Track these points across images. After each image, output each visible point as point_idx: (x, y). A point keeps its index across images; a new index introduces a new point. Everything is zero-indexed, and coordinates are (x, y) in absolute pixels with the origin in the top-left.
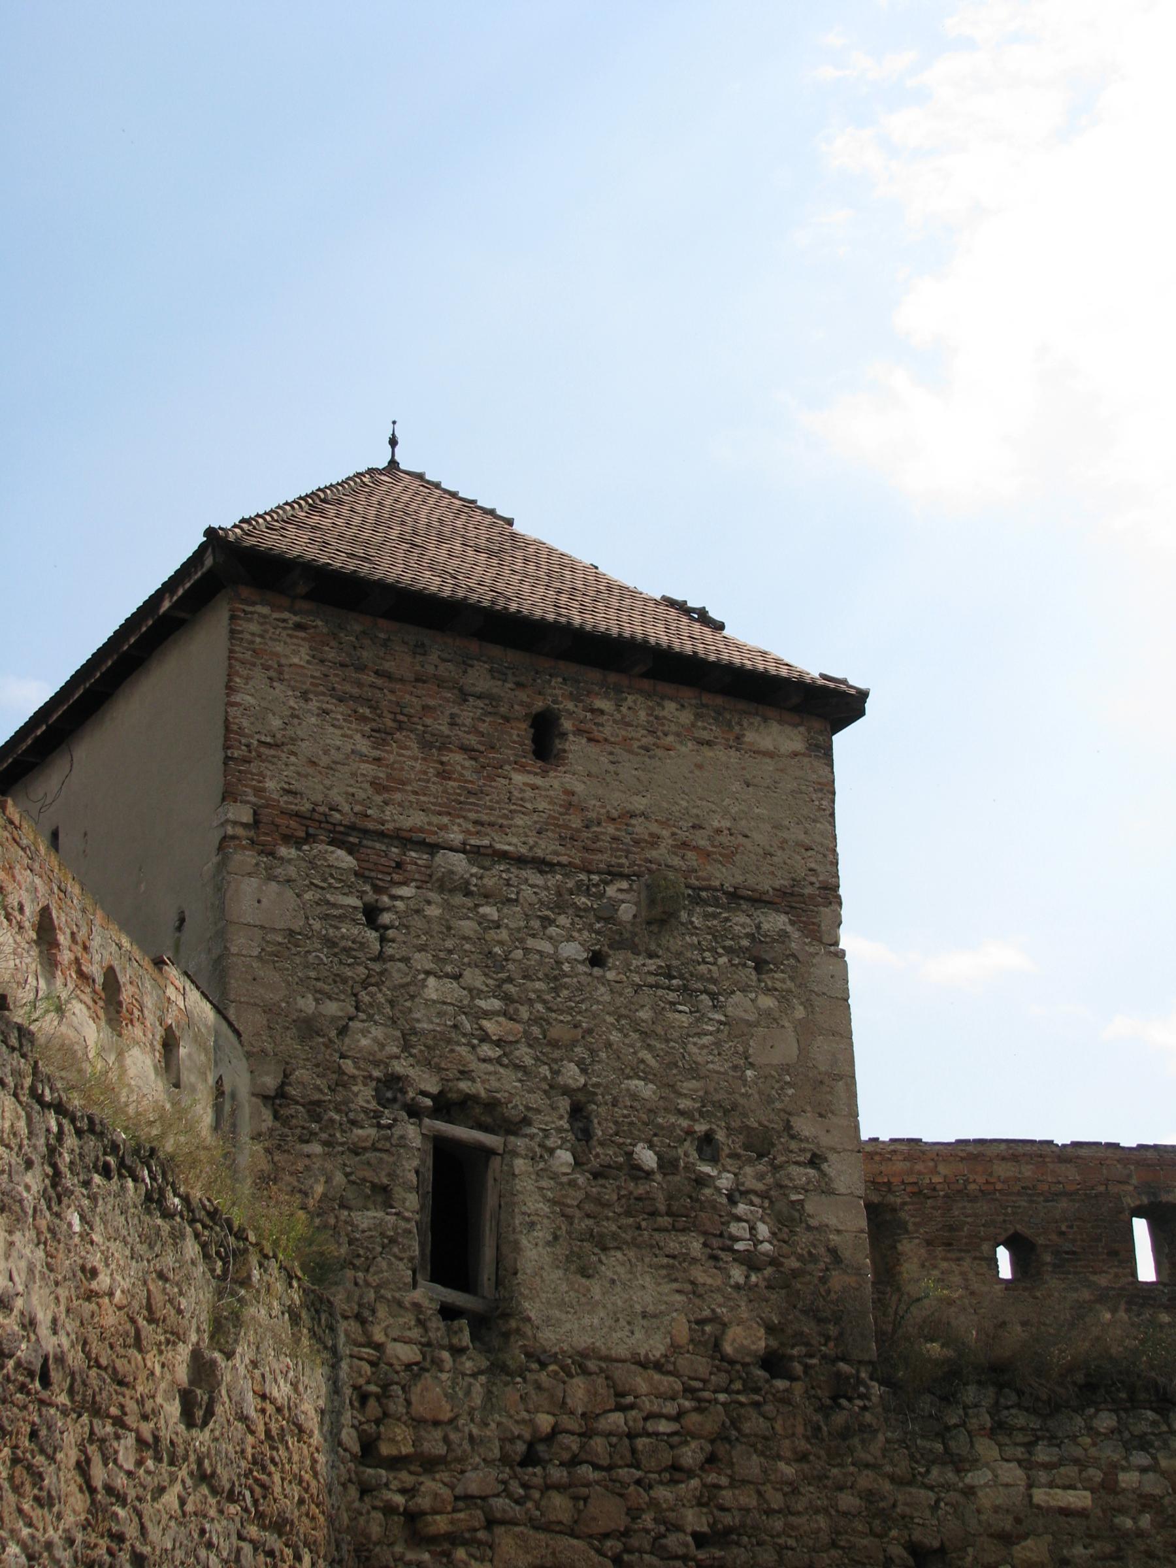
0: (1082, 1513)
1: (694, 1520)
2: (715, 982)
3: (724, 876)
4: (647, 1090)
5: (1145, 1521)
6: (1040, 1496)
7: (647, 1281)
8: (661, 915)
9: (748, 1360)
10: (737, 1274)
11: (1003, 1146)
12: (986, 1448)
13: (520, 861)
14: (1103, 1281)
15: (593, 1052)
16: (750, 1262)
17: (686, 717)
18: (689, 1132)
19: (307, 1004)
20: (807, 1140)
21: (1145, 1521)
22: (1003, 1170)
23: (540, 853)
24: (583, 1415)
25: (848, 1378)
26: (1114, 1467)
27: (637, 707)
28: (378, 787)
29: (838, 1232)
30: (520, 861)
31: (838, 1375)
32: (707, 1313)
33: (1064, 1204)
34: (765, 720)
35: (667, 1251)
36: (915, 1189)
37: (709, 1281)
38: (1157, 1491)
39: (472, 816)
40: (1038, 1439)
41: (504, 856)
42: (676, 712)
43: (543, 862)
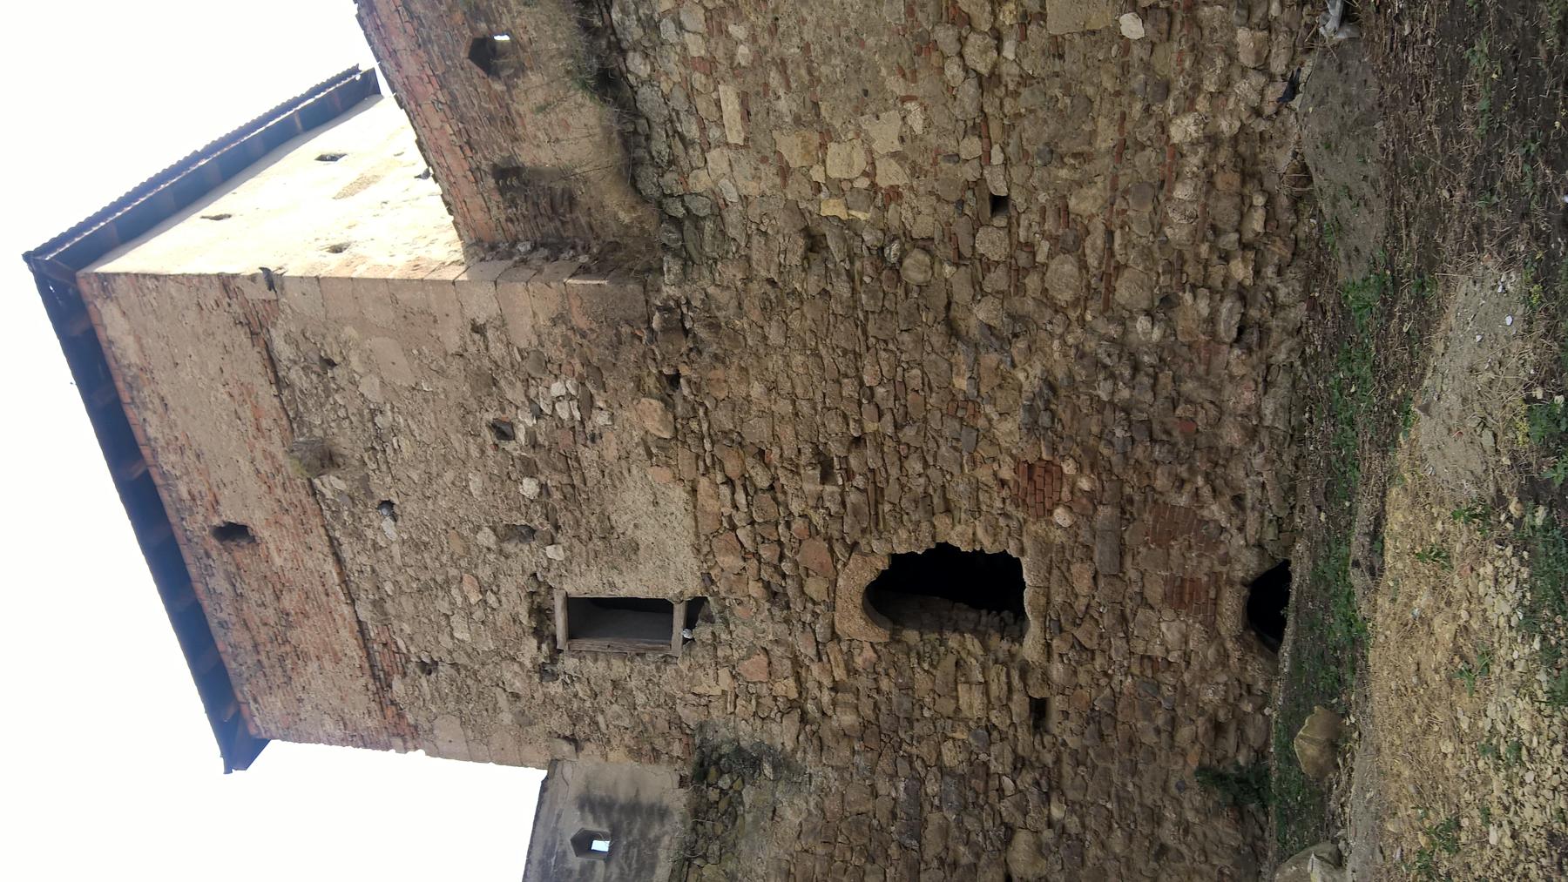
0: (744, 99)
2: (362, 415)
3: (266, 393)
4: (476, 483)
5: (738, 31)
6: (735, 137)
7: (628, 497)
8: (327, 459)
9: (671, 417)
10: (601, 419)
11: (444, 747)
13: (339, 561)
16: (587, 404)
19: (507, 718)
20: (462, 338)
21: (738, 31)
22: (411, 67)
23: (326, 550)
24: (744, 559)
25: (665, 320)
26: (685, 60)
27: (168, 461)
29: (535, 314)
30: (339, 561)
31: (664, 330)
32: (641, 450)
34: (111, 342)
35: (599, 476)
36: (466, 148)
37: (613, 445)
39: (324, 598)
40: (676, 131)
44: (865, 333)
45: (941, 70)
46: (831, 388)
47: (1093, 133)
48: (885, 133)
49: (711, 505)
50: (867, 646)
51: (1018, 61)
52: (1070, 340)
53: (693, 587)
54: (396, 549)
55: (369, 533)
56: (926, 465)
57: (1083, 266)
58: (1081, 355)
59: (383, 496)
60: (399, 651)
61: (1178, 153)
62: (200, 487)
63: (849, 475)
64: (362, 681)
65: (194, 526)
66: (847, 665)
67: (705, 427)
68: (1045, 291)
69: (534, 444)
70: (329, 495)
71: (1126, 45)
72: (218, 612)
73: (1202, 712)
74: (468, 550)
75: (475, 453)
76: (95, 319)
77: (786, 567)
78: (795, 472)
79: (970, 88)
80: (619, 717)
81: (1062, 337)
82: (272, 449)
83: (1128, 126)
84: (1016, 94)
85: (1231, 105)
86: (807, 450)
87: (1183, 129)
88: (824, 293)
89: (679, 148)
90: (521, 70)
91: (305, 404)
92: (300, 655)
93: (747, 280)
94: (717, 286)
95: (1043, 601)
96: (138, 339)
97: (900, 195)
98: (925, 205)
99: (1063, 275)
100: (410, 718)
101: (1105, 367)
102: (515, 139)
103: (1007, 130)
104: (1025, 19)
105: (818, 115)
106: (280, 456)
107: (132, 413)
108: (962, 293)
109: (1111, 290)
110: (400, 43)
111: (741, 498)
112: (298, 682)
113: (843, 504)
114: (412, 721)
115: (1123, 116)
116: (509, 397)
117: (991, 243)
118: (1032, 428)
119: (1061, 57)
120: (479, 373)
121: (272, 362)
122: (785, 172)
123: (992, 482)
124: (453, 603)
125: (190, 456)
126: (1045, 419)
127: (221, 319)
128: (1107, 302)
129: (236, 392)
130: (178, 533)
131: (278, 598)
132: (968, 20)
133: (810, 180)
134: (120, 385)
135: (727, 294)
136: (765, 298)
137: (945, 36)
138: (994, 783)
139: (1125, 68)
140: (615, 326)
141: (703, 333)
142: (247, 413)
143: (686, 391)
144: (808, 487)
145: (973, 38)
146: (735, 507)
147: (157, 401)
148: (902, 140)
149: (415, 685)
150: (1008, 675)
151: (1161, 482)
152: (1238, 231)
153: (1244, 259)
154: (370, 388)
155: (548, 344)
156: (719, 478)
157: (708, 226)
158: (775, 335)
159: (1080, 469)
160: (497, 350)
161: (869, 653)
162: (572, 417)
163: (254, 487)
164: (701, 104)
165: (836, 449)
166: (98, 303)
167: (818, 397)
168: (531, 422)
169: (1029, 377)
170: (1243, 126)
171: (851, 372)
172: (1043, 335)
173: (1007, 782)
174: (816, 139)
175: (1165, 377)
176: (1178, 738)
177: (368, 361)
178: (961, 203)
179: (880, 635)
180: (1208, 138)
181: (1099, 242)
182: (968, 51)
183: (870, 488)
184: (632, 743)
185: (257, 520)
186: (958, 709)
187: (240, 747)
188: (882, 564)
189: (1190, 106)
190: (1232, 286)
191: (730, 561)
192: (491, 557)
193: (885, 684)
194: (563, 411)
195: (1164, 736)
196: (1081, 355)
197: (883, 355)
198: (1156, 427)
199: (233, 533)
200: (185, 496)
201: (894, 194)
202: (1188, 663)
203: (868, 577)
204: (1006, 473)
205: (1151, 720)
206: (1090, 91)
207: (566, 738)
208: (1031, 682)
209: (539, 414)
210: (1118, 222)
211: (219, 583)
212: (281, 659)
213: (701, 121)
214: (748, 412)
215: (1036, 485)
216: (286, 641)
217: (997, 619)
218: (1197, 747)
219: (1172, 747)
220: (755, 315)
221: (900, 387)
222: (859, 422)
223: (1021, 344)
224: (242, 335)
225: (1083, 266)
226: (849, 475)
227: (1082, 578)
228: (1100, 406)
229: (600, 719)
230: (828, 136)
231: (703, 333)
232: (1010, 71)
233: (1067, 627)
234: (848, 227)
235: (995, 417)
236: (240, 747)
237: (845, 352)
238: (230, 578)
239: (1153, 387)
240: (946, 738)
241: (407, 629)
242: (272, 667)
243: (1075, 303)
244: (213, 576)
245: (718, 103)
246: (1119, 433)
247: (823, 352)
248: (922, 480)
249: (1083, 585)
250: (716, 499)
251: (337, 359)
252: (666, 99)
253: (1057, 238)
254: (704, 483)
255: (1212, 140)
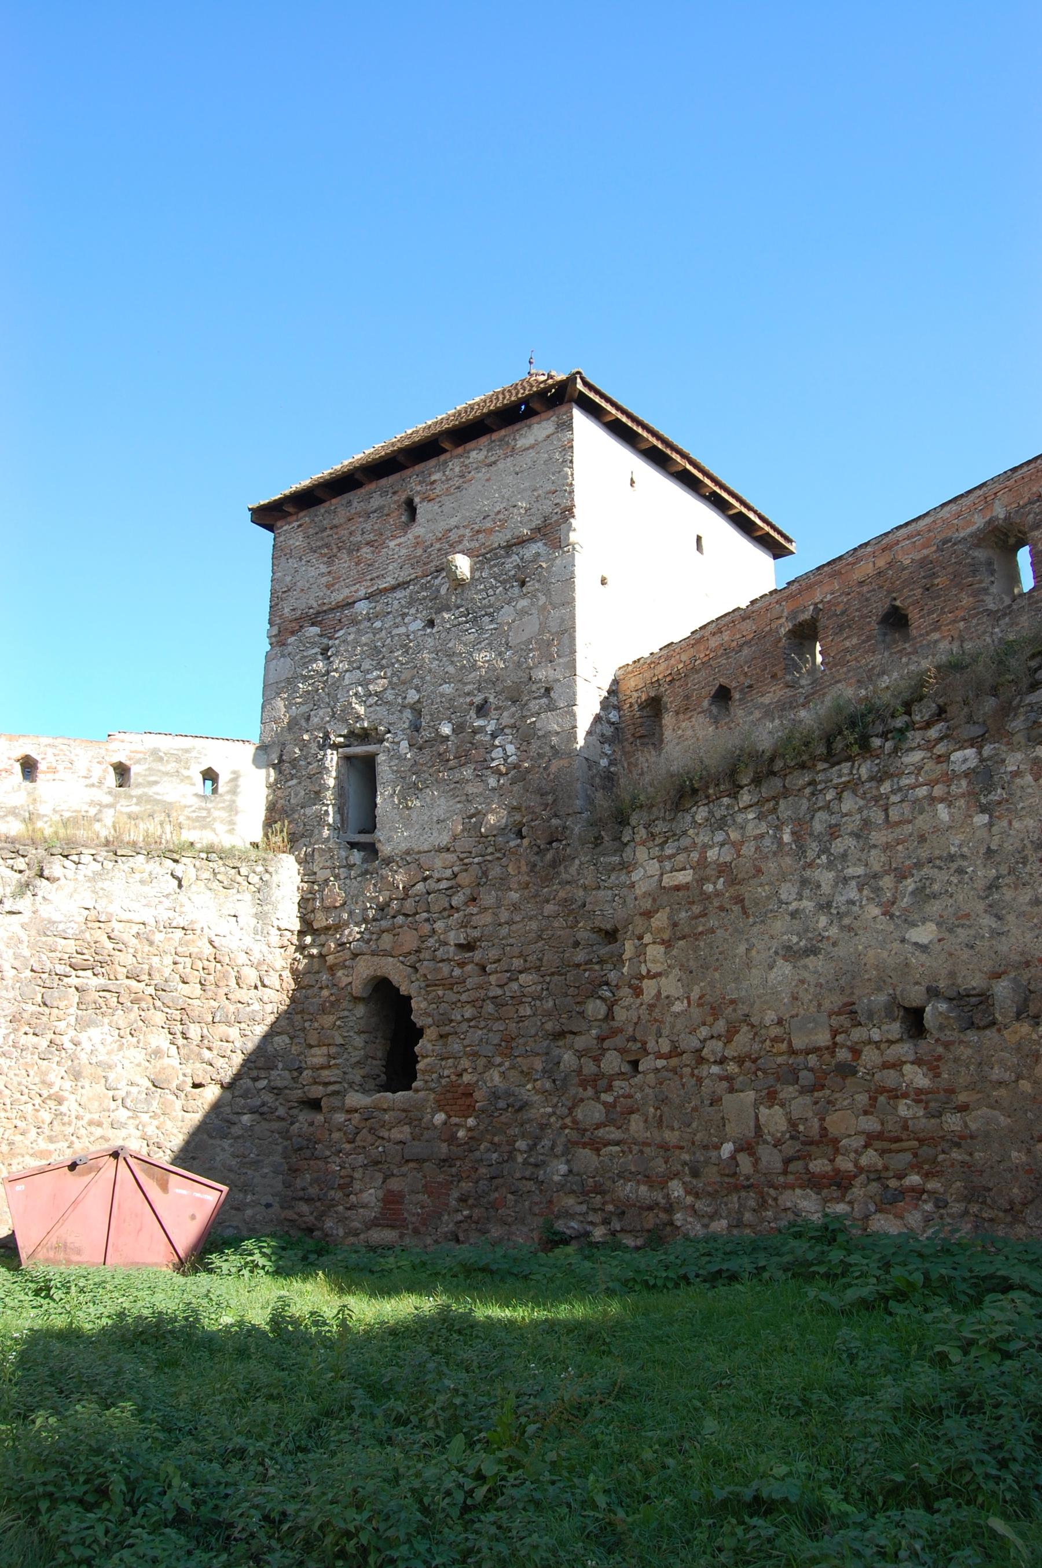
0: (686, 887)
1: (455, 937)
2: (490, 606)
3: (499, 539)
4: (447, 689)
10: (492, 782)
12: (642, 854)
13: (394, 588)
14: (766, 700)
15: (422, 678)
17: (481, 456)
18: (472, 704)
22: (713, 643)
23: (401, 579)
26: (706, 847)
27: (455, 466)
28: (328, 586)
30: (394, 588)
33: (746, 651)
34: (529, 427)
38: (728, 859)
40: (668, 838)
41: (386, 590)
42: (477, 453)
43: (404, 583)
44: (552, 974)
45: (704, 1024)
46: (516, 951)
47: (673, 1129)
48: (670, 986)
49: (438, 863)
50: (350, 979)
51: (710, 1075)
52: (553, 1119)
53: (386, 850)
54: (402, 630)
55: (413, 611)
56: (469, 1020)
57: (598, 1126)
58: (543, 1127)
59: (437, 621)
60: (336, 632)
61: (663, 1185)
62: (439, 488)
63: (462, 965)
64: (315, 605)
65: (412, 482)
66: (335, 965)
67: (489, 858)
68: (582, 1100)
69: (475, 732)
70: (437, 582)
71: (718, 1147)
72: (356, 500)
73: (319, 1218)
74: (404, 683)
75: (468, 688)
76: (544, 416)
77: (400, 919)
78: (463, 925)
79: (696, 1044)
80: (296, 795)
81: (554, 1113)
82: (465, 542)
83: (677, 1152)
84: (692, 1075)
85: (690, 1219)
86: (476, 934)
87: (676, 1189)
88: (576, 944)
89: (658, 841)
90: (716, 721)
91: (495, 566)
92: (331, 560)
93: (585, 888)
94: (580, 868)
95: (385, 1106)
96: (532, 447)
97: (638, 996)
98: (633, 1015)
99: (592, 1112)
100: (291, 640)
101: (535, 1145)
102: (677, 713)
103: (674, 1071)
104: (729, 1078)
105: (679, 939)
106: (203, 805)
107: (484, 440)
108: (580, 1042)
109: (585, 1145)
110: (726, 636)
111: (444, 885)
112: (313, 557)
113: (443, 961)
114: (289, 641)
115: (682, 1148)
116: (505, 714)
117: (612, 1063)
118: (495, 1095)
119: (711, 1105)
120: (520, 693)
121: (522, 542)
122: (648, 914)
123: (460, 1068)
124: (368, 672)
125: (457, 481)
126: (502, 1104)
127: (547, 507)
128: (576, 1143)
129: (501, 516)
130: (408, 472)
131: (367, 544)
132: (729, 1041)
133: (644, 933)
134: (503, 432)
135: (575, 873)
136: (573, 901)
137: (721, 1026)
138: (263, 1074)
139: (706, 1147)
140: (553, 791)
141: (549, 856)
142: (488, 524)
143: (512, 844)
144: (452, 934)
145: (720, 1044)
146: (439, 880)
147: (493, 459)
148: (667, 997)
149: (314, 644)
150: (335, 1082)
151: (466, 1186)
152: (622, 1230)
153: (605, 1235)
154: (507, 614)
155: (539, 743)
156: (456, 869)
157: (616, 859)
158: (550, 908)
159: (470, 1129)
160: (534, 705)
161: (345, 981)
162: (493, 760)
163: (442, 525)
164: (681, 858)
165: (477, 955)
166: (554, 418)
167: (511, 941)
168: (489, 729)
169: (527, 1091)
170: (678, 1228)
171: (528, 965)
172: (555, 1100)
173: (263, 1083)
174: (666, 937)
175: (530, 1186)
176: (301, 1203)
177: (523, 613)
178: (635, 1040)
179: (357, 989)
180: (671, 1205)
181: (612, 1136)
182: (714, 1041)
183: (453, 981)
184: (279, 806)
185: (418, 530)
186: (311, 1046)
187: (267, 516)
188: (403, 991)
189: (688, 1193)
190: (589, 1228)
191: (400, 879)
192: (400, 700)
193: (325, 993)
194: (497, 753)
195: (301, 1193)
196: (543, 1127)
197: (539, 987)
198: (500, 1181)
199: (411, 509)
200: (433, 478)
201: (638, 992)
202: (349, 1209)
203: (395, 979)
204: (466, 1078)
205: (311, 1184)
206: (694, 1125)
207: (281, 755)
208: (331, 1099)
209: (494, 736)
210: (626, 1149)
211: (376, 501)
212: (327, 546)
213: (673, 856)
214: (499, 889)
215: (458, 1098)
216: (339, 549)
217: (377, 1072)
218: (296, 1217)
219: (294, 1199)
220: (562, 894)
221: (518, 1000)
222: (496, 972)
223: (548, 1085)
224: (537, 522)
225: (598, 1126)
226: (462, 965)
227: (402, 1133)
228: (512, 1142)
229: (294, 782)
230: (668, 944)
231: (549, 856)
232: (704, 1070)
233: (368, 1123)
234: (618, 960)
235: (503, 1069)
236: (267, 516)
237: (540, 960)
238: (381, 508)
239: (524, 1178)
240: (291, 1038)
241: (351, 638)
242: (322, 539)
243: (575, 1122)
244: (377, 497)
245: (684, 869)
246: (495, 1156)
247: (540, 944)
248: (459, 1018)
249: (396, 1134)
250: (441, 865)
251: (524, 590)
252: (685, 833)
253: (615, 1107)
254: (451, 857)
255: (669, 1209)
